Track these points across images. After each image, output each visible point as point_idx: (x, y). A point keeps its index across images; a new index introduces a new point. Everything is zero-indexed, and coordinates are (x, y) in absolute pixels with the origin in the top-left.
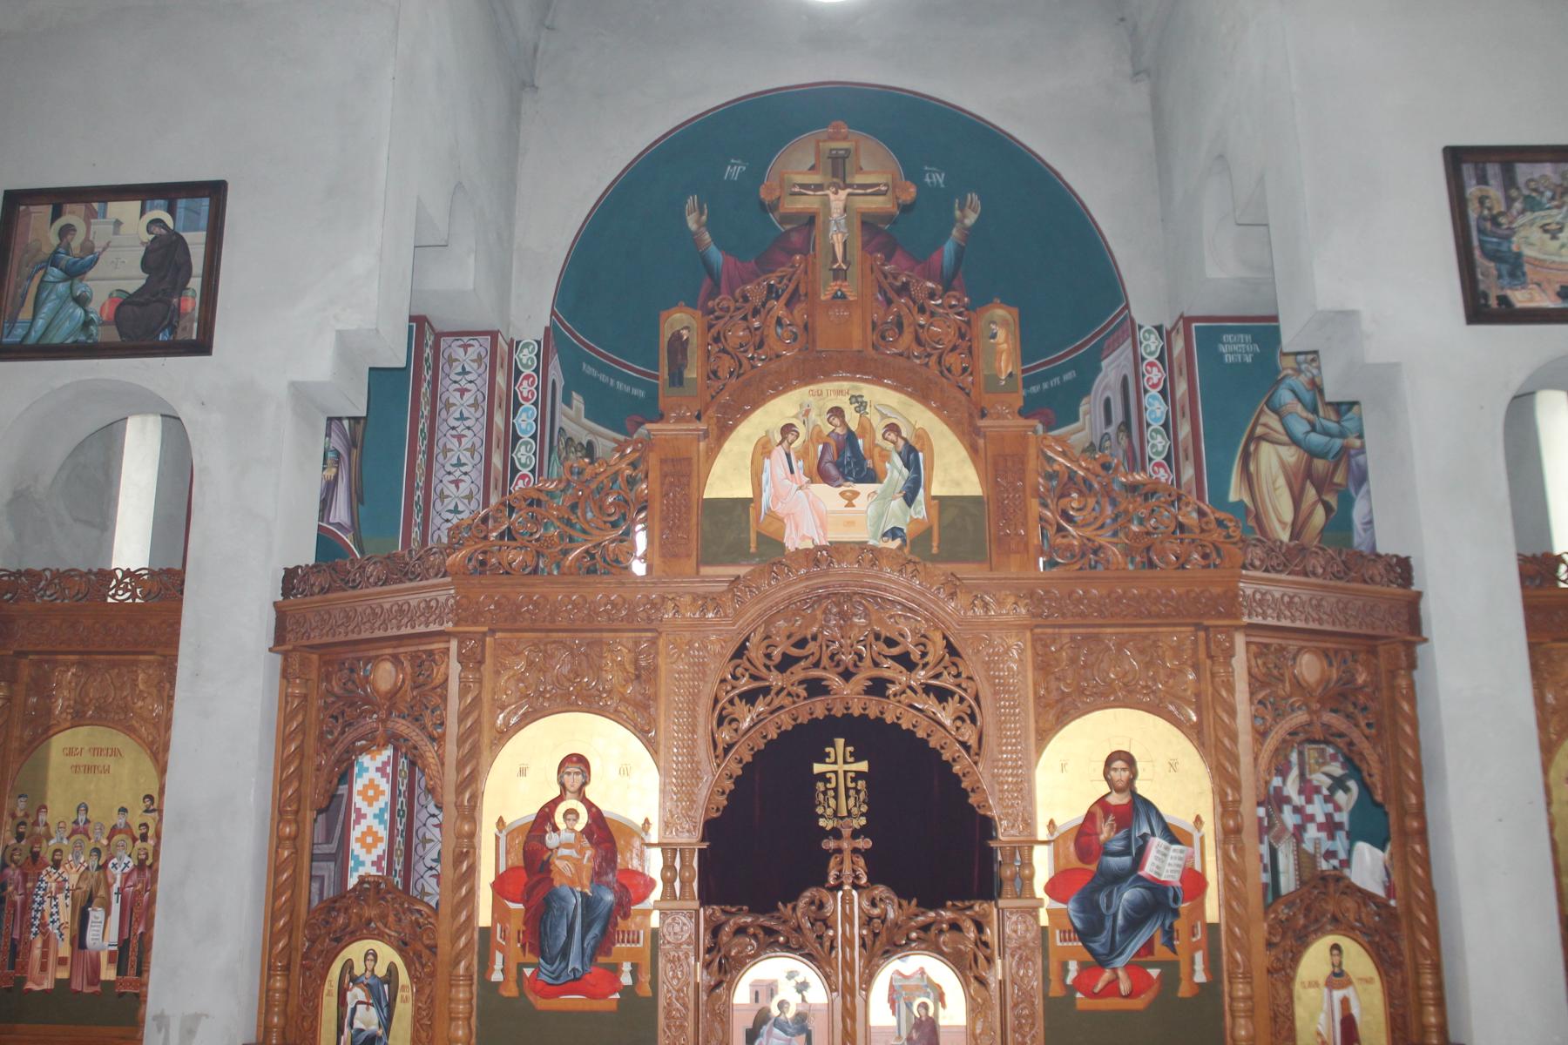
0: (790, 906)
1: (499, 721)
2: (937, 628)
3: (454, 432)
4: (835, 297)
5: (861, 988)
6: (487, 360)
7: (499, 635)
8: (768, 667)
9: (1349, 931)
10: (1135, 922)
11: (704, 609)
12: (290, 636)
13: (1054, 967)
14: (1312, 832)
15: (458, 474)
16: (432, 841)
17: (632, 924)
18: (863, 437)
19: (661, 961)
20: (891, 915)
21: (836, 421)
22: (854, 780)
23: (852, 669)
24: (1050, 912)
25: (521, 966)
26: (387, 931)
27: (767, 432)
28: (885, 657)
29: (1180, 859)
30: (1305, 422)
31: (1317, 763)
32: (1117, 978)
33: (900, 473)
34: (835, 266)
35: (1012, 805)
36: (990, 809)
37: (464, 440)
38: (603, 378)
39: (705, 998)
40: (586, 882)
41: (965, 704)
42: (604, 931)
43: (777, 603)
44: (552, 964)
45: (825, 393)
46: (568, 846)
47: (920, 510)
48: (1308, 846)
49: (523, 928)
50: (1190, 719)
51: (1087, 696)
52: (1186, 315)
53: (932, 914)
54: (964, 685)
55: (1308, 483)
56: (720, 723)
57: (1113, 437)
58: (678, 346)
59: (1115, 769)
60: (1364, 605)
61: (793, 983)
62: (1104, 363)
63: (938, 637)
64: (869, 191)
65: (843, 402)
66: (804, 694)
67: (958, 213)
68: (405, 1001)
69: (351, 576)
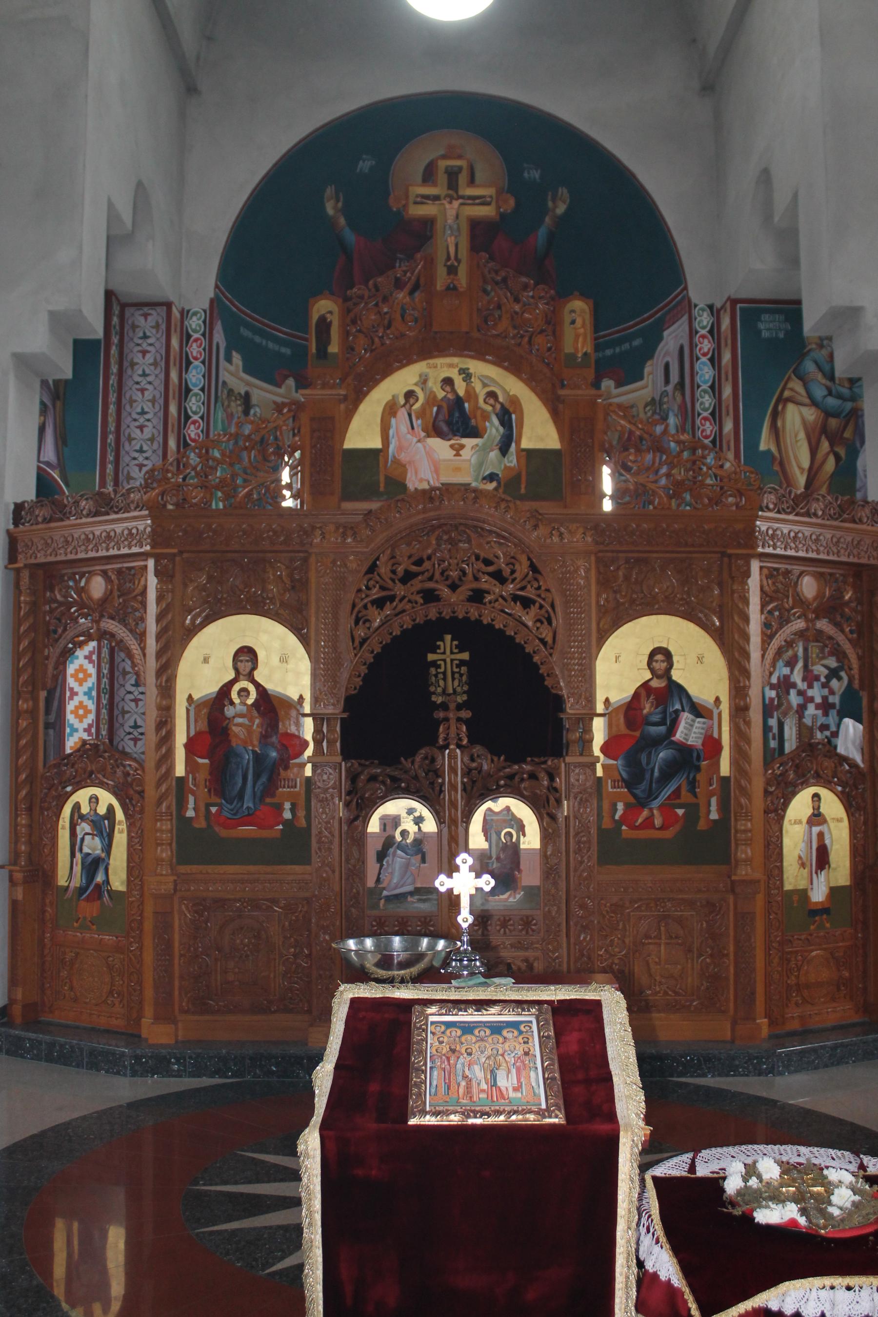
0: (410, 760)
1: (188, 622)
2: (523, 552)
3: (138, 387)
4: (448, 288)
5: (463, 822)
6: (164, 326)
7: (185, 555)
8: (393, 580)
9: (827, 784)
10: (667, 776)
11: (344, 536)
12: (20, 557)
13: (606, 805)
14: (811, 710)
15: (142, 420)
16: (129, 712)
17: (291, 774)
18: (468, 401)
19: (313, 802)
20: (485, 767)
21: (448, 388)
22: (458, 666)
23: (457, 582)
24: (603, 766)
25: (208, 806)
26: (105, 780)
27: (393, 396)
28: (484, 573)
29: (703, 729)
30: (824, 388)
31: (817, 656)
32: (653, 815)
33: (497, 430)
34: (449, 263)
35: (578, 687)
36: (561, 690)
37: (146, 393)
38: (257, 339)
39: (346, 828)
40: (256, 742)
41: (543, 611)
42: (270, 779)
43: (400, 532)
44: (231, 804)
45: (439, 366)
46: (241, 716)
47: (512, 460)
48: (808, 721)
49: (209, 777)
50: (714, 624)
51: (637, 605)
52: (733, 297)
53: (516, 767)
54: (543, 596)
55: (823, 437)
56: (357, 622)
57: (670, 394)
58: (324, 325)
59: (657, 661)
60: (853, 540)
61: (412, 817)
62: (666, 333)
63: (523, 559)
64: (477, 201)
65: (454, 374)
66: (421, 601)
67: (550, 204)
68: (121, 832)
69: (68, 509)
